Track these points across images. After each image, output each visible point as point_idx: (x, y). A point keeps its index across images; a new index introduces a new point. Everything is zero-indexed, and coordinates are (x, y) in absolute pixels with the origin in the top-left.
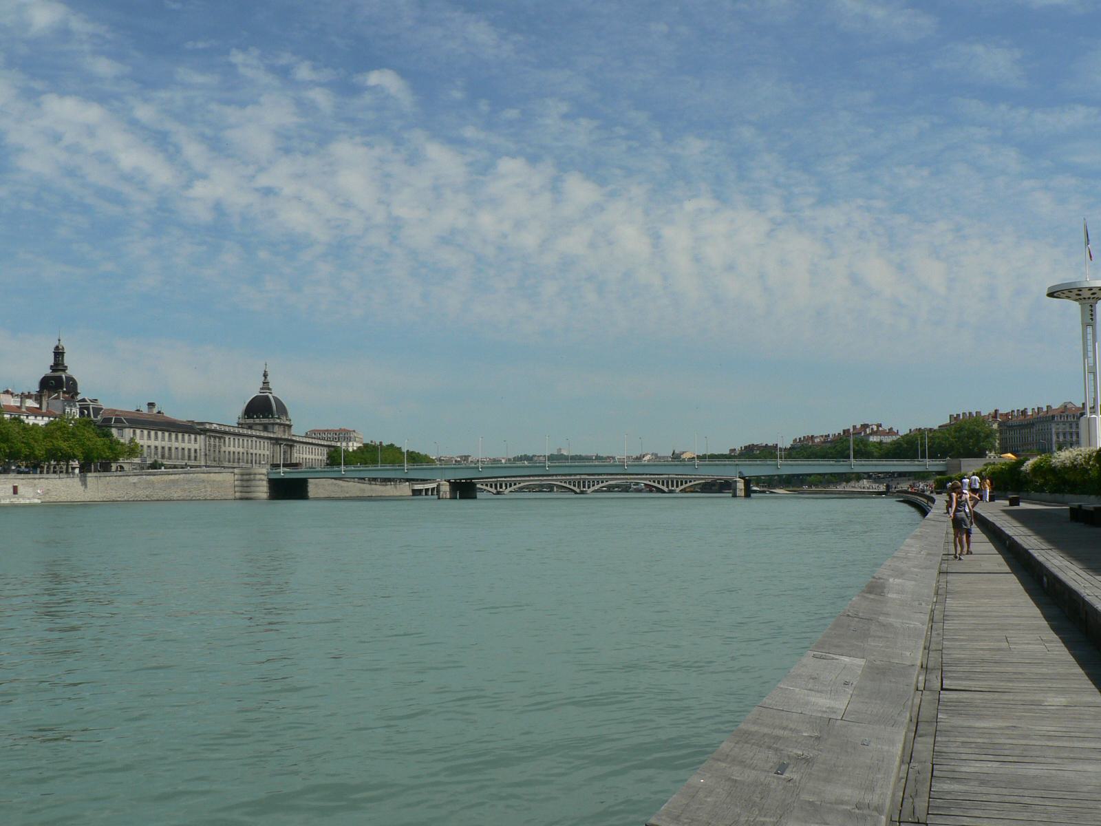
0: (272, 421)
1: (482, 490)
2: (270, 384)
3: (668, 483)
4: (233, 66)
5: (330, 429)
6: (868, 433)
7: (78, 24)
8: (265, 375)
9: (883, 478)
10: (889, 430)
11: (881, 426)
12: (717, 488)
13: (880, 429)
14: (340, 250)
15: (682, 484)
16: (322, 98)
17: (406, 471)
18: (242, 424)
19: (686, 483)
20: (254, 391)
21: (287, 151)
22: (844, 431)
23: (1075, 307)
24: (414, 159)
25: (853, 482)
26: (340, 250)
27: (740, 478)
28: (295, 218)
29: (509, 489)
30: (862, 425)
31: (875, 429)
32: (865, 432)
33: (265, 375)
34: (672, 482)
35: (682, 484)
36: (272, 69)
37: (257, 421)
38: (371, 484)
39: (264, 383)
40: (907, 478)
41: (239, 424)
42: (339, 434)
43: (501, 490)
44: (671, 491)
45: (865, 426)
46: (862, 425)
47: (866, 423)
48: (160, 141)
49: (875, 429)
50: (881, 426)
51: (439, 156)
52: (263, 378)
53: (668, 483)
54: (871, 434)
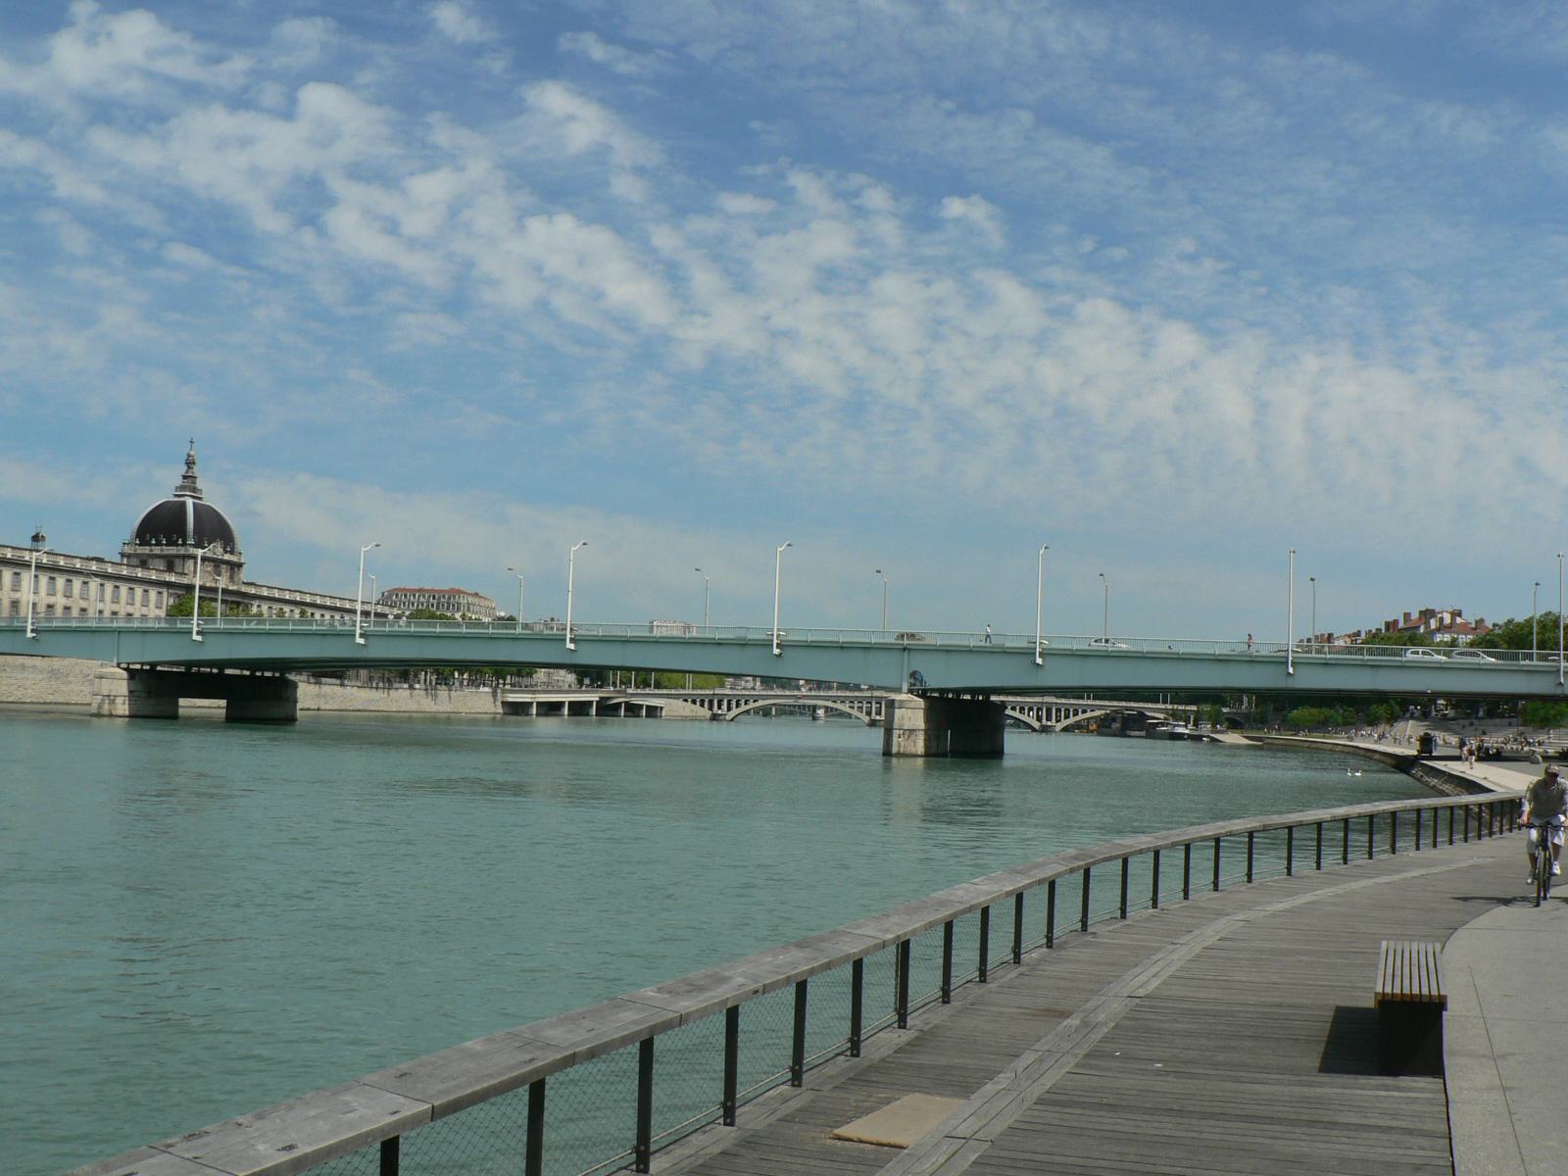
0: (182, 551)
1: (1019, 724)
2: (198, 480)
3: (711, 703)
4: (792, 190)
5: (436, 588)
6: (1433, 627)
7: (617, 141)
8: (190, 463)
9: (1454, 719)
10: (1476, 622)
11: (1460, 615)
12: (1116, 726)
13: (1459, 620)
14: (857, 405)
15: (738, 706)
16: (889, 231)
17: (29, 635)
18: (129, 556)
19: (1076, 714)
20: (161, 489)
21: (823, 290)
22: (1388, 625)
23: (1508, 1093)
24: (979, 299)
25: (1383, 725)
26: (857, 405)
27: (911, 691)
28: (802, 363)
29: (735, 711)
30: (1421, 612)
31: (1447, 619)
32: (1427, 624)
33: (190, 463)
34: (1049, 711)
35: (738, 706)
36: (840, 195)
37: (157, 550)
38: (320, 683)
39: (185, 477)
40: (1506, 721)
41: (123, 555)
42: (439, 598)
43: (1049, 723)
44: (1045, 730)
45: (1427, 614)
46: (1421, 612)
47: (1430, 608)
48: (673, 276)
49: (1447, 619)
50: (1460, 615)
51: (1012, 296)
52: (186, 468)
53: (711, 703)
54: (1438, 630)
